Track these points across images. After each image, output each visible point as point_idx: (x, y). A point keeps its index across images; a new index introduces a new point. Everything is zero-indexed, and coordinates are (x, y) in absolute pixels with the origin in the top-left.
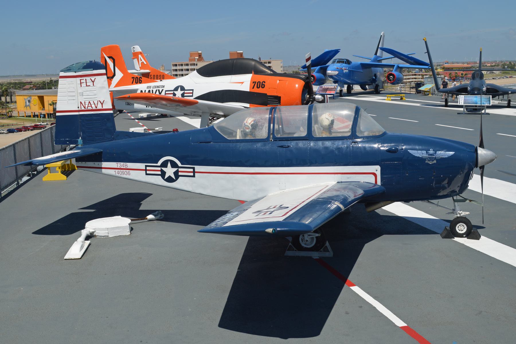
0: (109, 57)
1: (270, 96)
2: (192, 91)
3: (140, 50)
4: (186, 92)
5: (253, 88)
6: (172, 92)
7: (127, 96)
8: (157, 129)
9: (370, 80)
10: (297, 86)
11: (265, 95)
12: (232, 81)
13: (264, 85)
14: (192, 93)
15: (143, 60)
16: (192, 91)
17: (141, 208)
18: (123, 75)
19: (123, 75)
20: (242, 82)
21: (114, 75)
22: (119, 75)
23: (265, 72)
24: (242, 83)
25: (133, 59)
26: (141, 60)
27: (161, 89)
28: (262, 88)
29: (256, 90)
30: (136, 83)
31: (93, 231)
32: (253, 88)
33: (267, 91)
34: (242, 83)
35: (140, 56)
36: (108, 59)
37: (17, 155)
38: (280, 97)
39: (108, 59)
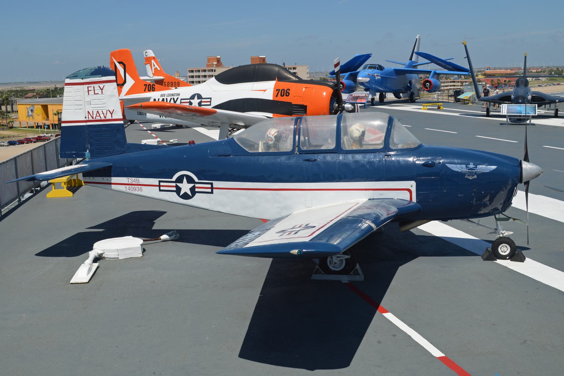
0: (119, 63)
1: (295, 105)
2: (209, 100)
3: (153, 55)
4: (203, 100)
5: (277, 96)
6: (188, 101)
7: (139, 104)
8: (172, 141)
9: (404, 88)
10: (325, 94)
11: (290, 104)
12: (253, 89)
13: (289, 93)
14: (210, 102)
15: (156, 66)
16: (209, 100)
17: (154, 228)
18: (134, 82)
19: (134, 82)
20: (265, 90)
21: (125, 82)
22: (130, 82)
23: (289, 79)
24: (265, 91)
25: (146, 64)
26: (154, 66)
27: (176, 98)
28: (287, 96)
29: (280, 99)
30: (149, 91)
31: (102, 252)
32: (277, 96)
33: (292, 99)
34: (265, 91)
35: (153, 61)
36: (118, 65)
37: (18, 169)
38: (306, 106)
39: (118, 65)
